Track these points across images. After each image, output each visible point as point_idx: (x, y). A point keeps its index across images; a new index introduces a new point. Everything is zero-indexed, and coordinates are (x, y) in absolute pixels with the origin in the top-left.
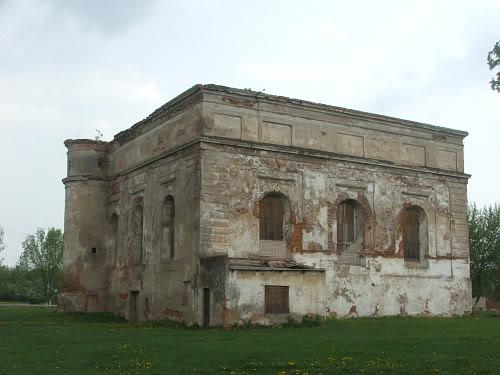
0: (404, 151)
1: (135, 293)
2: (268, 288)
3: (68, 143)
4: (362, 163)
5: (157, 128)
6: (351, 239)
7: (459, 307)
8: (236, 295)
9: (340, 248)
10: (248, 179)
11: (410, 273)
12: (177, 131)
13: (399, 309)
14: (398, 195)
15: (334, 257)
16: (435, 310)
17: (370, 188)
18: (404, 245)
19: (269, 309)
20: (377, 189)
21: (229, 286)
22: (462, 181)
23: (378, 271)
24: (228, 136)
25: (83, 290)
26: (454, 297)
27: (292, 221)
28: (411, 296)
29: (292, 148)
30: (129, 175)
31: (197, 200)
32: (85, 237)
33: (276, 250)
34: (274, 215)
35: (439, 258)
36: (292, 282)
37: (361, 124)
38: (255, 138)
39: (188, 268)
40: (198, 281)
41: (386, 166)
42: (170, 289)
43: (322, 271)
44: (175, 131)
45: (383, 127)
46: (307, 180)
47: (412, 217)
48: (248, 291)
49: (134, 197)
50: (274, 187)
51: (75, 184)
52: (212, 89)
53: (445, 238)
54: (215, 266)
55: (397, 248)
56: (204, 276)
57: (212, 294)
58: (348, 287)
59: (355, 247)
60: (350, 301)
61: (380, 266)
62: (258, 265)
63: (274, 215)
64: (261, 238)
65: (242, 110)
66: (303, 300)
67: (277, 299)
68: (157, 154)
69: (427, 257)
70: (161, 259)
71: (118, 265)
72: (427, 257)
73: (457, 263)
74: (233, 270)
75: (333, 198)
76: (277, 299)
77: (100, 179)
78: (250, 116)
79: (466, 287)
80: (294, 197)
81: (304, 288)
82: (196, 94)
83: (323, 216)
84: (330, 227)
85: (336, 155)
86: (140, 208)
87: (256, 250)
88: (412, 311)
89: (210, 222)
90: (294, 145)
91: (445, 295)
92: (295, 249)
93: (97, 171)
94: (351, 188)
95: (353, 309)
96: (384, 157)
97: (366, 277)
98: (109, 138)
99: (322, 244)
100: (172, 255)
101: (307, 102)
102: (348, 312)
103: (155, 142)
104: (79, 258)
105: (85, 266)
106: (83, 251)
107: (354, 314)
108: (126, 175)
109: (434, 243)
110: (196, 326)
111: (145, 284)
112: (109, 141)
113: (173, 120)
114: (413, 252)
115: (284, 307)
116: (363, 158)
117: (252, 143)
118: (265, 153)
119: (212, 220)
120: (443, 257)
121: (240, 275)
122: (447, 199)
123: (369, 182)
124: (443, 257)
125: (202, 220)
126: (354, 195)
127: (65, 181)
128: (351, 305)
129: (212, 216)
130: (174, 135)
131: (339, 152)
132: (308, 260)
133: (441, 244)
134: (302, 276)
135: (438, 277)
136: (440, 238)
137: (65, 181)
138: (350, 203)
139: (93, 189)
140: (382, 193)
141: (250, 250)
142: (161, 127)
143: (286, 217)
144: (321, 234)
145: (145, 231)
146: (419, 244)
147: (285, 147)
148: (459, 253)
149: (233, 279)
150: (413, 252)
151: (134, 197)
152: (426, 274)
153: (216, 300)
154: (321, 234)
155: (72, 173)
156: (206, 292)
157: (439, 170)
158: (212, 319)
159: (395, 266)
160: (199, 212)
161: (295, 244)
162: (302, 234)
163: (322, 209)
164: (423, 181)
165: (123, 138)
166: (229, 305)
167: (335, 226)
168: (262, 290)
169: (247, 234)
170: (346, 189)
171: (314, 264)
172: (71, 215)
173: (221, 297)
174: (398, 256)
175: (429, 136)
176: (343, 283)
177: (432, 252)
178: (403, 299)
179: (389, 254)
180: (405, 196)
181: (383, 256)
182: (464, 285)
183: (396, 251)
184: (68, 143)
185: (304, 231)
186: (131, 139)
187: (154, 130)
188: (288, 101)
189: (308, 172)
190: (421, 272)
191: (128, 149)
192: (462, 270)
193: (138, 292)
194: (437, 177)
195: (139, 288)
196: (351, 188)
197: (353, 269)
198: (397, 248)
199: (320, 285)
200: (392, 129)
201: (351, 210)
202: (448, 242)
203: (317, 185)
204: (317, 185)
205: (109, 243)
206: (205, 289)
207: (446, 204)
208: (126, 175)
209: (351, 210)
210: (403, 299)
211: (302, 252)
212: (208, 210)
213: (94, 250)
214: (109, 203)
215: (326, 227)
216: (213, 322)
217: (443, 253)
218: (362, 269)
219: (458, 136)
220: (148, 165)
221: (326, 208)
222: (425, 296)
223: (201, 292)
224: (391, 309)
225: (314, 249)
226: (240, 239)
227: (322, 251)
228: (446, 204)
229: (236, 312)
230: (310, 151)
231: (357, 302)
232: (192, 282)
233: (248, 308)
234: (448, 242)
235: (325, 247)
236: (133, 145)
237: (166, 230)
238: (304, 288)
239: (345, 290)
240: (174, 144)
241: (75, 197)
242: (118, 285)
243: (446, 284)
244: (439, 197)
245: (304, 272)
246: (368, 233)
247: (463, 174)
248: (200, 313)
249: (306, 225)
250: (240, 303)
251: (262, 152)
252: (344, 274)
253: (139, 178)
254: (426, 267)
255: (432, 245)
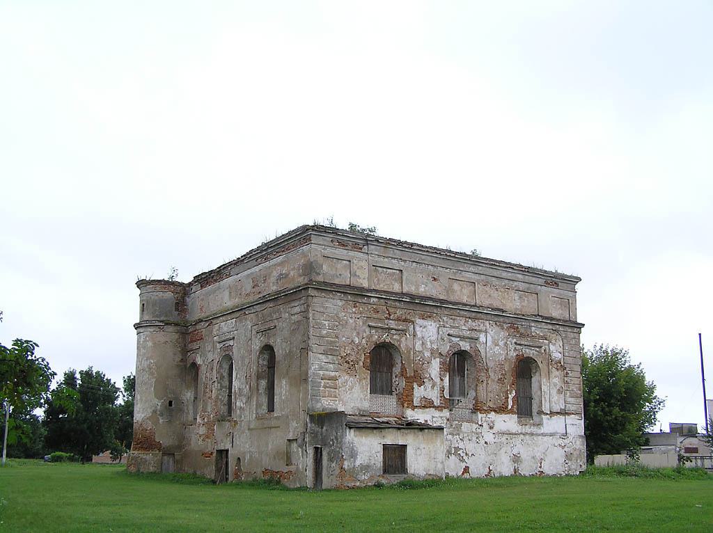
0: (517, 298)
1: (223, 453)
2: (385, 447)
3: (141, 284)
4: (476, 312)
5: (253, 270)
6: (463, 393)
7: (573, 467)
8: (353, 455)
9: (449, 404)
10: (351, 328)
11: (523, 431)
12: (287, 269)
13: (512, 470)
14: (512, 347)
15: (446, 413)
16: (548, 469)
17: (482, 338)
18: (516, 399)
19: (387, 469)
20: (489, 338)
21: (347, 445)
22: (575, 330)
23: (491, 428)
24: (337, 281)
25: (158, 446)
26: (569, 456)
27: (403, 373)
28: (524, 456)
29: (403, 294)
30: (214, 321)
31: (305, 350)
32: (162, 387)
33: (387, 406)
34: (383, 363)
35: (552, 414)
36: (410, 440)
37: (472, 269)
38: (365, 284)
39: (295, 424)
40: (307, 440)
41: (498, 315)
42: (270, 447)
43: (441, 429)
44: (275, 274)
45: (496, 273)
46: (418, 328)
47: (524, 369)
48: (367, 450)
49: (219, 346)
50: (385, 337)
51: (151, 329)
52: (318, 229)
53: (559, 392)
54: (327, 423)
55: (510, 403)
56: (314, 435)
57: (325, 453)
58: (461, 445)
59: (467, 403)
60: (462, 460)
61: (492, 422)
62: (372, 425)
63: (383, 363)
64: (373, 391)
65: (352, 253)
66: (423, 458)
67: (395, 457)
68: (251, 299)
69: (541, 412)
70: (257, 413)
71: (199, 420)
72: (541, 412)
73: (572, 419)
74: (350, 428)
75: (445, 349)
76: (395, 457)
77: (176, 325)
78: (360, 260)
79: (580, 445)
80: (404, 343)
81: (422, 446)
82: (304, 234)
83: (435, 368)
84: (442, 380)
85: (451, 303)
86: (229, 358)
87: (366, 405)
88: (526, 470)
89: (318, 375)
90: (404, 291)
91: (559, 454)
92: (406, 405)
93: (174, 317)
94: (463, 338)
95: (466, 470)
96: (496, 304)
97: (479, 436)
98: (186, 277)
99: (434, 399)
100: (271, 408)
101: (418, 245)
102: (460, 473)
103: (248, 287)
104: (155, 412)
105: (161, 421)
106: (159, 403)
107: (467, 476)
108: (211, 320)
109: (547, 397)
110: (303, 489)
111: (237, 442)
112: (186, 282)
113: (272, 262)
114: (525, 408)
115: (402, 468)
116: (475, 306)
117: (362, 289)
118: (375, 300)
119: (321, 372)
120: (558, 413)
121: (357, 433)
122: (561, 350)
123: (480, 331)
124: (558, 413)
125: (310, 372)
126: (465, 346)
127: (137, 326)
128: (463, 465)
129: (321, 368)
130: (273, 279)
131: (452, 299)
132: (420, 416)
133: (555, 397)
134: (420, 433)
135: (552, 435)
136: (554, 392)
137: (137, 326)
138: (461, 356)
139: (170, 334)
140: (494, 345)
141: (359, 405)
142: (257, 269)
143: (397, 370)
144: (433, 387)
145: (235, 384)
146: (531, 399)
147: (396, 294)
148: (572, 408)
149: (351, 436)
150: (525, 408)
151: (219, 346)
152: (540, 431)
153: (331, 460)
154: (433, 387)
155: (146, 318)
156: (318, 452)
157: (552, 319)
158: (325, 479)
159: (508, 422)
160: (307, 363)
161: (406, 399)
162: (413, 388)
163: (433, 361)
164: (535, 330)
165: (204, 279)
166: (346, 465)
167: (447, 379)
168: (380, 449)
169: (357, 389)
170: (458, 339)
171: (426, 421)
172: (145, 364)
173: (336, 457)
174: (511, 412)
175: (541, 281)
176: (456, 441)
177: (546, 408)
178: (516, 459)
179: (502, 409)
180: (518, 347)
181: (495, 411)
182: (578, 443)
183: (510, 407)
184: (141, 284)
185: (415, 386)
186: (216, 281)
187: (249, 272)
188: (400, 243)
189: (419, 321)
190: (534, 430)
191: (208, 294)
192: (576, 426)
193: (227, 451)
194: (550, 327)
195: (228, 446)
196: (463, 338)
197: (466, 427)
198: (510, 403)
199: (438, 442)
200: (504, 275)
201: (460, 363)
202: (562, 396)
203: (428, 336)
204: (428, 336)
205: (188, 395)
206: (316, 449)
207: (560, 356)
208: (211, 320)
209: (460, 363)
210: (516, 459)
211: (414, 408)
212: (318, 363)
213: (170, 404)
214: (185, 351)
215: (438, 380)
216: (326, 482)
217: (556, 408)
218: (475, 426)
219: (571, 282)
220: (239, 311)
221: (438, 360)
222: (538, 455)
223: (311, 452)
224: (505, 468)
225: (427, 404)
226: (353, 395)
227: (434, 407)
228: (560, 356)
229: (353, 473)
230: (422, 298)
231: (470, 462)
232: (300, 441)
233: (366, 468)
234: (562, 396)
235: (437, 402)
236: (219, 288)
237: (263, 383)
238: (422, 446)
239: (457, 449)
240: (274, 288)
241: (150, 344)
242: (200, 442)
243: (560, 441)
244: (552, 348)
245: (422, 429)
246: (480, 388)
247: (576, 323)
248: (310, 474)
249: (418, 378)
250: (358, 463)
251: (372, 300)
252: (457, 431)
253: (226, 326)
254: (539, 425)
255: (545, 400)
